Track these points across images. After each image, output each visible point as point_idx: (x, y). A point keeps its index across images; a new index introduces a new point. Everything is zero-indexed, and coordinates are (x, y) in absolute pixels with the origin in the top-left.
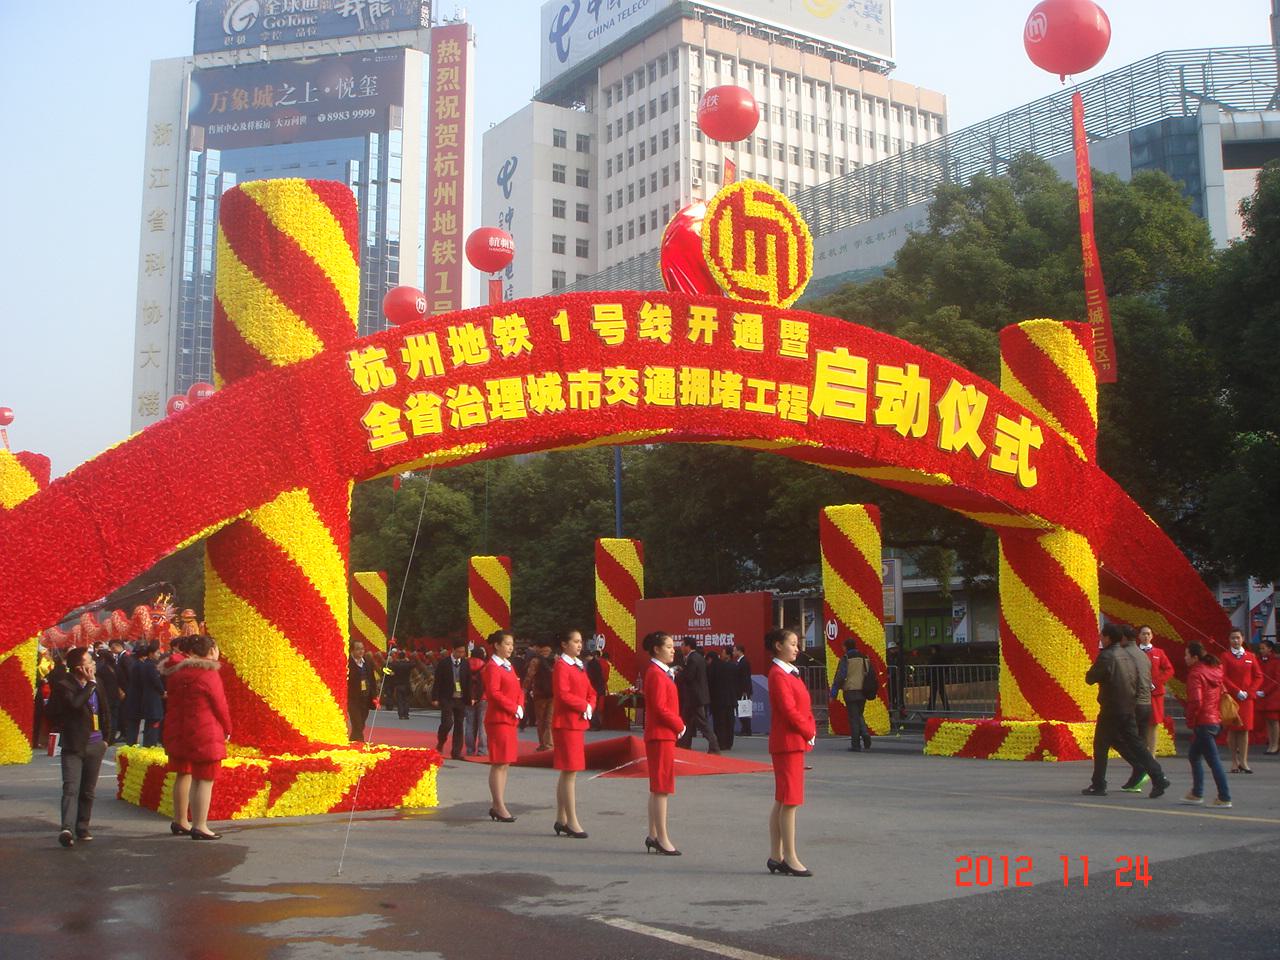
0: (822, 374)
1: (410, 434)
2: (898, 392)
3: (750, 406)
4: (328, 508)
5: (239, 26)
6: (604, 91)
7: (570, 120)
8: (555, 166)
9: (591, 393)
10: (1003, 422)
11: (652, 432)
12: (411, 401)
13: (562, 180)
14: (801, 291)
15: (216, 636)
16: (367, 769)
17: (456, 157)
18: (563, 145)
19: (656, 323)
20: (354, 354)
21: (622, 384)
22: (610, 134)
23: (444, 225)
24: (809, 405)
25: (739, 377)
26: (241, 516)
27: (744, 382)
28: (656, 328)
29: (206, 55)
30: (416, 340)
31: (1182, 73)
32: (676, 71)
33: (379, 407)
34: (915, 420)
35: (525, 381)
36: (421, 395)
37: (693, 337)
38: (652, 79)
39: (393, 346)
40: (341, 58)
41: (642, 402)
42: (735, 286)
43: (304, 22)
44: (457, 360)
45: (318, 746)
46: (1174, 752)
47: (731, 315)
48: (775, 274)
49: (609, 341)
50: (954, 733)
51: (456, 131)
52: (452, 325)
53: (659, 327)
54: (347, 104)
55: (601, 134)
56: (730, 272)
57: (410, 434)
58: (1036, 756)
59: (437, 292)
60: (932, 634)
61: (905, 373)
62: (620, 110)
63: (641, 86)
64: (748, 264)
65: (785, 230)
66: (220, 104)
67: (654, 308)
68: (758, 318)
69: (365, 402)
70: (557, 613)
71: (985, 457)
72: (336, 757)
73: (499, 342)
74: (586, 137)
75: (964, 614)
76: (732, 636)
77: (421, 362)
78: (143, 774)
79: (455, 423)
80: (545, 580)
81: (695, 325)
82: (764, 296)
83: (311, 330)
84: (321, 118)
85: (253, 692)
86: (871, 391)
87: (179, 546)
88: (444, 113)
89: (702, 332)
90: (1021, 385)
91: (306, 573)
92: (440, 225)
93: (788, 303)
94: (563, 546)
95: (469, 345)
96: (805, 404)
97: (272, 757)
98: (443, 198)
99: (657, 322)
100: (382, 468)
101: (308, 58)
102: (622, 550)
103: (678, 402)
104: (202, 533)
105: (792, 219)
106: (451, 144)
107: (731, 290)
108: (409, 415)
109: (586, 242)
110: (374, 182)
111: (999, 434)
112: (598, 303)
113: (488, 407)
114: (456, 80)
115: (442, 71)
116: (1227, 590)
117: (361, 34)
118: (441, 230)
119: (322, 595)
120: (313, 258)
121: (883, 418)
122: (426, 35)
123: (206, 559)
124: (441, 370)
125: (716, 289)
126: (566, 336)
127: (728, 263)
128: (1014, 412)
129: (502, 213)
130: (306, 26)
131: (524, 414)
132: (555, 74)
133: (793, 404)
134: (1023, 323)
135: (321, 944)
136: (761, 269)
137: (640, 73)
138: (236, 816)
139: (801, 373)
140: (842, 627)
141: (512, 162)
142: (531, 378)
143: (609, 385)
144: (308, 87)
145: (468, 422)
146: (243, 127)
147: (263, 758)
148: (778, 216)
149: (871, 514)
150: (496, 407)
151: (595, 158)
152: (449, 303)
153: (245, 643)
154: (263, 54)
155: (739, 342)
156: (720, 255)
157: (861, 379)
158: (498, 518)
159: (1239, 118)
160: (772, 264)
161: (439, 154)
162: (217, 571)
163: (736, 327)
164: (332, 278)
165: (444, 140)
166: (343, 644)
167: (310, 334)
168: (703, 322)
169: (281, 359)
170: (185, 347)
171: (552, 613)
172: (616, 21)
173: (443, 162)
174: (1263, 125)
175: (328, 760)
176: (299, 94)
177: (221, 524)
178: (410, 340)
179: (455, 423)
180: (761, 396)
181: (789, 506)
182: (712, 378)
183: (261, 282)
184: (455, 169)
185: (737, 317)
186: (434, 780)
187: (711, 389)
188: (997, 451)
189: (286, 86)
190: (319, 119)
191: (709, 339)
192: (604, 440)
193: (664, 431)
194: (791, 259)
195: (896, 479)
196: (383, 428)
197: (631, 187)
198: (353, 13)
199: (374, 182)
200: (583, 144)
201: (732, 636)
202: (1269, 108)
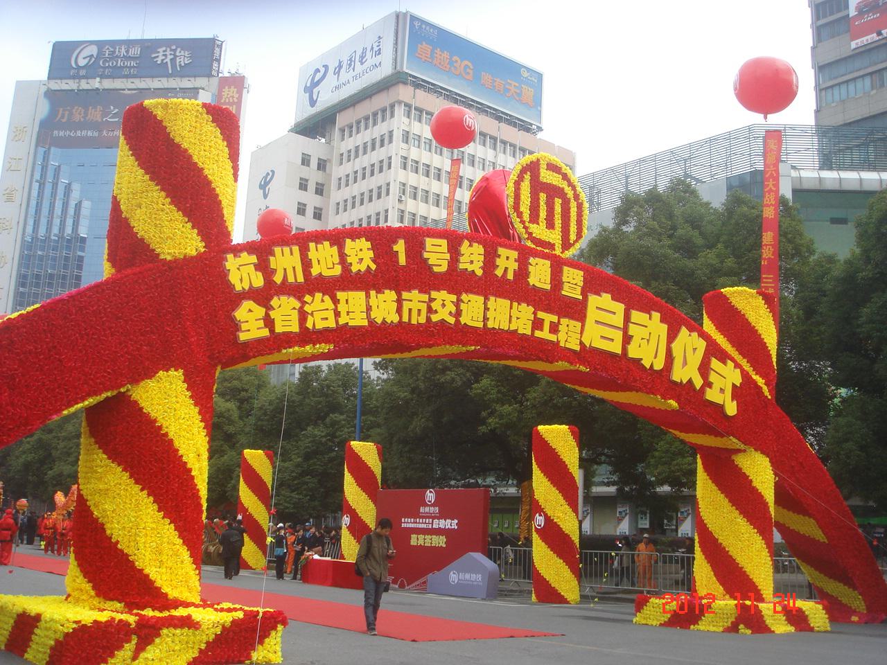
0: (592, 314)
1: (272, 330)
3: (538, 334)
4: (200, 392)
5: (82, 62)
6: (340, 129)
7: (316, 147)
8: (301, 179)
9: (419, 311)
10: (715, 364)
11: (464, 348)
12: (275, 302)
15: (89, 498)
16: (223, 626)
18: (308, 165)
19: (472, 258)
20: (230, 257)
21: (443, 305)
22: (342, 159)
24: (581, 337)
25: (531, 309)
26: (122, 390)
27: (535, 313)
28: (472, 262)
29: (56, 81)
30: (282, 250)
32: (392, 120)
33: (248, 304)
34: (655, 357)
35: (368, 296)
36: (284, 298)
37: (499, 272)
38: (375, 124)
40: (153, 92)
41: (458, 322)
43: (129, 65)
44: (315, 271)
45: (177, 604)
46: (829, 629)
47: (528, 259)
48: (560, 230)
49: (436, 269)
50: (656, 610)
52: (312, 241)
53: (474, 262)
55: (335, 160)
56: (527, 224)
57: (272, 330)
58: (733, 628)
60: (506, 526)
61: (650, 319)
62: (350, 143)
63: (366, 128)
64: (540, 220)
65: (568, 196)
66: (63, 117)
67: (471, 245)
68: (548, 263)
69: (236, 299)
70: (301, 497)
72: (197, 614)
73: (349, 260)
74: (325, 161)
75: (626, 514)
76: (456, 521)
77: (285, 269)
78: (12, 621)
79: (309, 325)
80: (293, 472)
81: (501, 263)
82: (552, 246)
85: (121, 551)
86: (625, 329)
87: (65, 412)
89: (506, 269)
90: (722, 336)
91: (176, 444)
93: (569, 254)
94: (306, 447)
95: (325, 260)
96: (579, 336)
97: (135, 611)
99: (473, 258)
100: (246, 358)
101: (129, 90)
102: (366, 451)
103: (485, 325)
104: (86, 403)
105: (574, 188)
107: (528, 239)
108: (273, 314)
111: (712, 372)
113: (337, 314)
117: (168, 76)
119: (189, 466)
120: (203, 169)
121: (633, 352)
122: (215, 81)
123: (84, 428)
124: (301, 279)
126: (402, 260)
127: (526, 217)
128: (724, 357)
129: (260, 209)
130: (130, 68)
131: (365, 323)
132: (306, 115)
133: (569, 335)
134: (725, 289)
136: (550, 225)
137: (367, 119)
139: (576, 310)
140: (548, 519)
141: (271, 174)
142: (373, 293)
143: (434, 306)
146: (79, 133)
148: (564, 185)
149: (573, 433)
150: (343, 314)
151: (330, 175)
153: (117, 505)
154: (96, 83)
155: (533, 280)
156: (521, 210)
157: (618, 320)
158: (259, 423)
159: (804, 174)
160: (558, 222)
162: (95, 438)
163: (531, 269)
164: (217, 189)
168: (507, 261)
169: (168, 253)
170: (22, 287)
171: (297, 496)
172: (351, 80)
174: (820, 179)
175: (189, 617)
177: (104, 396)
178: (277, 250)
179: (309, 325)
180: (547, 326)
181: (497, 425)
182: (511, 308)
183: (157, 185)
185: (532, 260)
186: (279, 639)
187: (510, 316)
188: (710, 385)
189: (112, 108)
191: (510, 276)
193: (473, 348)
195: (633, 402)
196: (250, 322)
197: (354, 198)
198: (165, 61)
200: (322, 165)
201: (456, 521)
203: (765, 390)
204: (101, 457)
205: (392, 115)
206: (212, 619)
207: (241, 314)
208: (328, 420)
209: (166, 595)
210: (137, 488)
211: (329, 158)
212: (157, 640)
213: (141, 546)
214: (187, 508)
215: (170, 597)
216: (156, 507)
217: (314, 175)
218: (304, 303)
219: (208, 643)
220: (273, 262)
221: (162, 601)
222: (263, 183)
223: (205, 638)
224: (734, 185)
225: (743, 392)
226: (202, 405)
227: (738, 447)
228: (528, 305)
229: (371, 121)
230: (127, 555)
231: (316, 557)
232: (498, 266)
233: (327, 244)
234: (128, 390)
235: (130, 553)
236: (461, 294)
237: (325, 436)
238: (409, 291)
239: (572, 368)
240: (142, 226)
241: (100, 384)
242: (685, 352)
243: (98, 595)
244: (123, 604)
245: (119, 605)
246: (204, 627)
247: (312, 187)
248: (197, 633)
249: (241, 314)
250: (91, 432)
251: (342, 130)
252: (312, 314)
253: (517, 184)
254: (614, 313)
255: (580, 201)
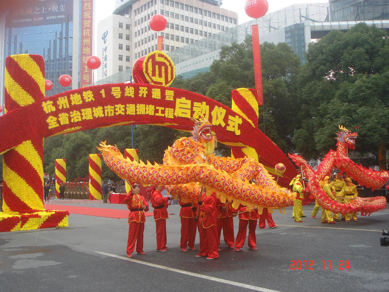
0: (178, 105)
2: (200, 109)
4: (38, 146)
7: (125, 19)
8: (119, 34)
9: (111, 112)
10: (230, 117)
12: (60, 115)
13: (122, 38)
14: (172, 82)
15: (6, 182)
16: (48, 217)
17: (90, 30)
18: (122, 27)
19: (130, 92)
20: (44, 103)
21: (120, 109)
23: (86, 51)
24: (174, 114)
25: (154, 106)
26: (12, 148)
27: (155, 108)
28: (130, 93)
31: (300, 11)
35: (92, 109)
37: (140, 95)
39: (54, 99)
41: (126, 114)
42: (153, 81)
44: (73, 104)
45: (35, 211)
51: (90, 22)
54: (56, 14)
56: (151, 77)
59: (84, 72)
61: (202, 104)
62: (139, 17)
63: (152, 6)
65: (167, 65)
68: (159, 90)
71: (225, 127)
72: (40, 213)
73: (85, 98)
77: (63, 104)
79: (72, 121)
82: (161, 83)
83: (31, 96)
84: (48, 18)
85: (17, 197)
86: (192, 109)
88: (86, 17)
89: (143, 94)
91: (31, 163)
92: (85, 51)
95: (76, 99)
97: (22, 214)
98: (86, 43)
105: (169, 62)
106: (88, 26)
108: (59, 119)
109: (129, 57)
110: (64, 38)
111: (229, 120)
112: (113, 87)
113: (82, 116)
114: (90, 7)
115: (85, 4)
116: (312, 161)
118: (85, 53)
119: (36, 169)
124: (68, 107)
125: (147, 82)
126: (104, 96)
127: (151, 75)
131: (92, 118)
133: (169, 113)
134: (238, 89)
135: (26, 260)
136: (160, 76)
137: (145, 5)
138: (12, 230)
139: (172, 105)
141: (106, 32)
142: (94, 108)
143: (116, 109)
144: (43, 8)
145: (76, 121)
147: (19, 215)
152: (88, 75)
156: (149, 72)
157: (189, 106)
159: (316, 24)
160: (163, 75)
161: (85, 29)
164: (37, 82)
165: (86, 25)
166: (42, 183)
167: (31, 98)
168: (143, 91)
173: (86, 32)
174: (323, 26)
175: (37, 214)
176: (41, 10)
178: (59, 98)
179: (72, 121)
180: (160, 112)
182: (146, 107)
183: (17, 83)
184: (90, 34)
185: (153, 90)
186: (67, 220)
187: (146, 110)
188: (229, 125)
189: (36, 8)
190: (47, 18)
191: (145, 96)
192: (116, 125)
193: (132, 122)
194: (169, 73)
196: (52, 122)
199: (64, 38)
200: (128, 27)
202: (325, 21)
203: (253, 124)
204: (8, 169)
205: (156, 4)
206: (44, 215)
207: (48, 121)
208: (125, 139)
209: (31, 209)
210: (20, 177)
211: (131, 23)
212: (28, 222)
213: (22, 195)
214: (36, 182)
215: (33, 209)
216: (26, 183)
217: (124, 32)
218: (70, 114)
219: (44, 222)
220: (58, 103)
221: (30, 210)
222: (103, 37)
223: (43, 220)
224: (288, 30)
225: (244, 126)
226: (38, 150)
227: (242, 146)
228: (152, 105)
229: (147, 6)
230: (19, 198)
231: (114, 193)
232: (140, 93)
233: (76, 94)
234: (14, 148)
235: (20, 197)
236: (126, 104)
237: (124, 146)
238: (107, 106)
239: (171, 124)
240: (13, 96)
241: (5, 147)
242: (217, 114)
243: (11, 210)
244: (18, 212)
245: (17, 213)
246: (42, 217)
247: (124, 37)
248: (40, 219)
249: (48, 121)
250: (5, 162)
251: (135, 11)
252: (73, 118)
253: (147, 64)
254: (187, 104)
255: (172, 66)
